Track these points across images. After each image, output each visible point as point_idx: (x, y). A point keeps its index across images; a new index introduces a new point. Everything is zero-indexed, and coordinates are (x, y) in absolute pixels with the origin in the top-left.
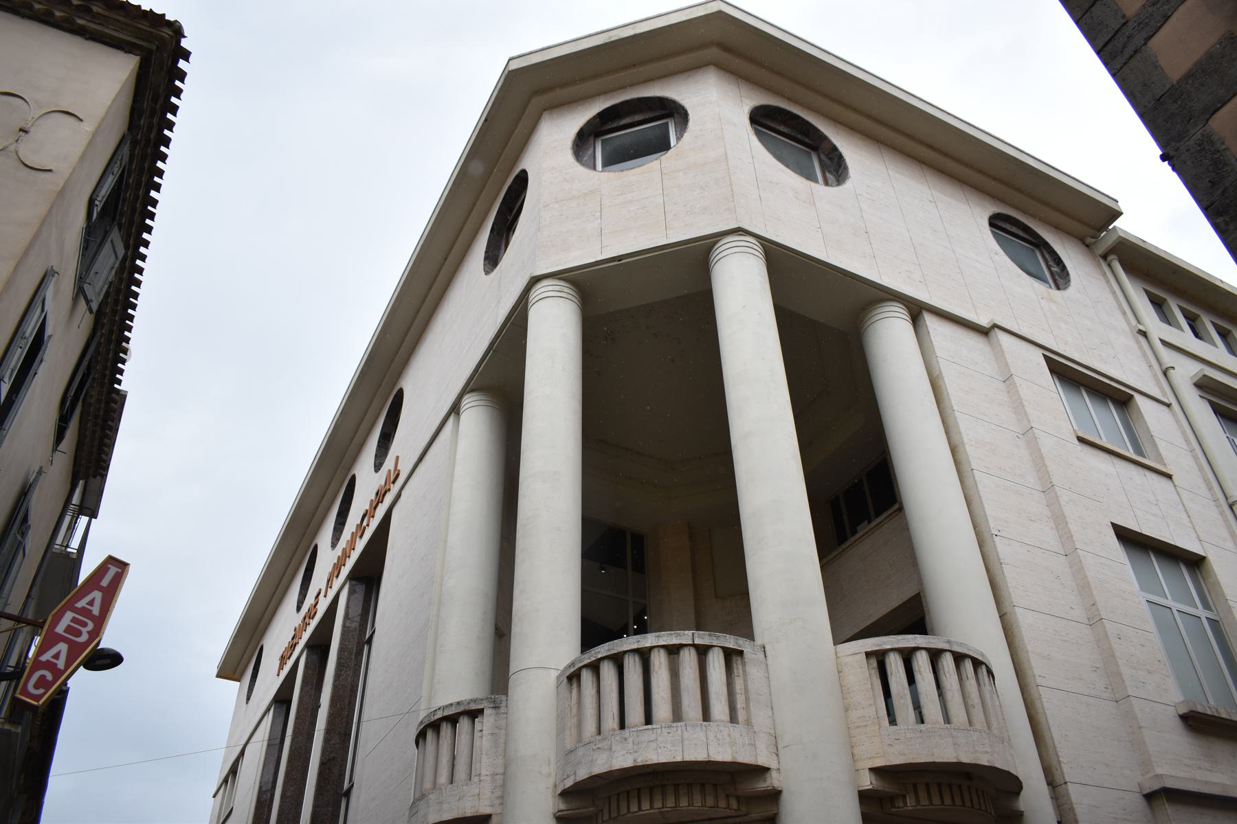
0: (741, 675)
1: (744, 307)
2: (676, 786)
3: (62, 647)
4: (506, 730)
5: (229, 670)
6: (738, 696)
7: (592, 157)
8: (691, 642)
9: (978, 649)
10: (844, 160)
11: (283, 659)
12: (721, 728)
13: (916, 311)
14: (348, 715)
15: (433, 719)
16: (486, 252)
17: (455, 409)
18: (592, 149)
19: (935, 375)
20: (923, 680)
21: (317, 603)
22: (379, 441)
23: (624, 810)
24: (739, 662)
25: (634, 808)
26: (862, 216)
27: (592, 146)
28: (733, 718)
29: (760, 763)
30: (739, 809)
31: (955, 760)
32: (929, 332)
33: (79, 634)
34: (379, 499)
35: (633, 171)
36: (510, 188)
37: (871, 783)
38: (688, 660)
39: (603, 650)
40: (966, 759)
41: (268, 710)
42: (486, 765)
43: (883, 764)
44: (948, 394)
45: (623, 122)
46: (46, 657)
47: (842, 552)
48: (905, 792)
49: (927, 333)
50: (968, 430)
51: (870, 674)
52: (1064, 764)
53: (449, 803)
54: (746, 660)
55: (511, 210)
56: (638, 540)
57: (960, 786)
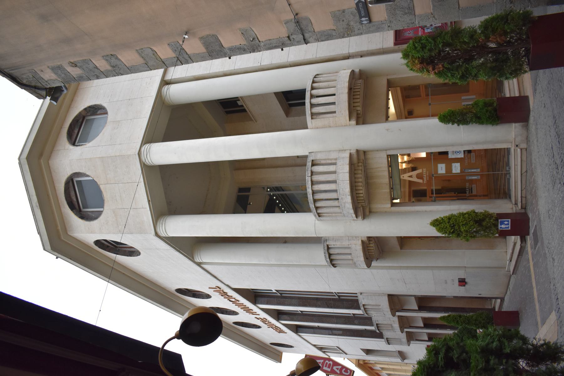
0: (320, 161)
1: (175, 153)
2: (355, 182)
3: (335, 368)
5: (277, 358)
6: (327, 162)
7: (93, 213)
8: (310, 177)
10: (91, 106)
11: (281, 331)
12: (338, 168)
14: (310, 299)
15: (329, 261)
16: (128, 256)
17: (199, 264)
18: (89, 213)
20: (321, 101)
22: (196, 298)
24: (315, 161)
26: (121, 101)
27: (87, 213)
28: (335, 164)
29: (349, 156)
30: (362, 163)
31: (347, 94)
33: (330, 364)
39: (312, 206)
41: (300, 336)
42: (346, 243)
45: (75, 199)
46: (338, 372)
47: (250, 113)
48: (356, 110)
53: (358, 254)
54: (315, 159)
55: (108, 246)
56: (241, 190)
57: (354, 92)
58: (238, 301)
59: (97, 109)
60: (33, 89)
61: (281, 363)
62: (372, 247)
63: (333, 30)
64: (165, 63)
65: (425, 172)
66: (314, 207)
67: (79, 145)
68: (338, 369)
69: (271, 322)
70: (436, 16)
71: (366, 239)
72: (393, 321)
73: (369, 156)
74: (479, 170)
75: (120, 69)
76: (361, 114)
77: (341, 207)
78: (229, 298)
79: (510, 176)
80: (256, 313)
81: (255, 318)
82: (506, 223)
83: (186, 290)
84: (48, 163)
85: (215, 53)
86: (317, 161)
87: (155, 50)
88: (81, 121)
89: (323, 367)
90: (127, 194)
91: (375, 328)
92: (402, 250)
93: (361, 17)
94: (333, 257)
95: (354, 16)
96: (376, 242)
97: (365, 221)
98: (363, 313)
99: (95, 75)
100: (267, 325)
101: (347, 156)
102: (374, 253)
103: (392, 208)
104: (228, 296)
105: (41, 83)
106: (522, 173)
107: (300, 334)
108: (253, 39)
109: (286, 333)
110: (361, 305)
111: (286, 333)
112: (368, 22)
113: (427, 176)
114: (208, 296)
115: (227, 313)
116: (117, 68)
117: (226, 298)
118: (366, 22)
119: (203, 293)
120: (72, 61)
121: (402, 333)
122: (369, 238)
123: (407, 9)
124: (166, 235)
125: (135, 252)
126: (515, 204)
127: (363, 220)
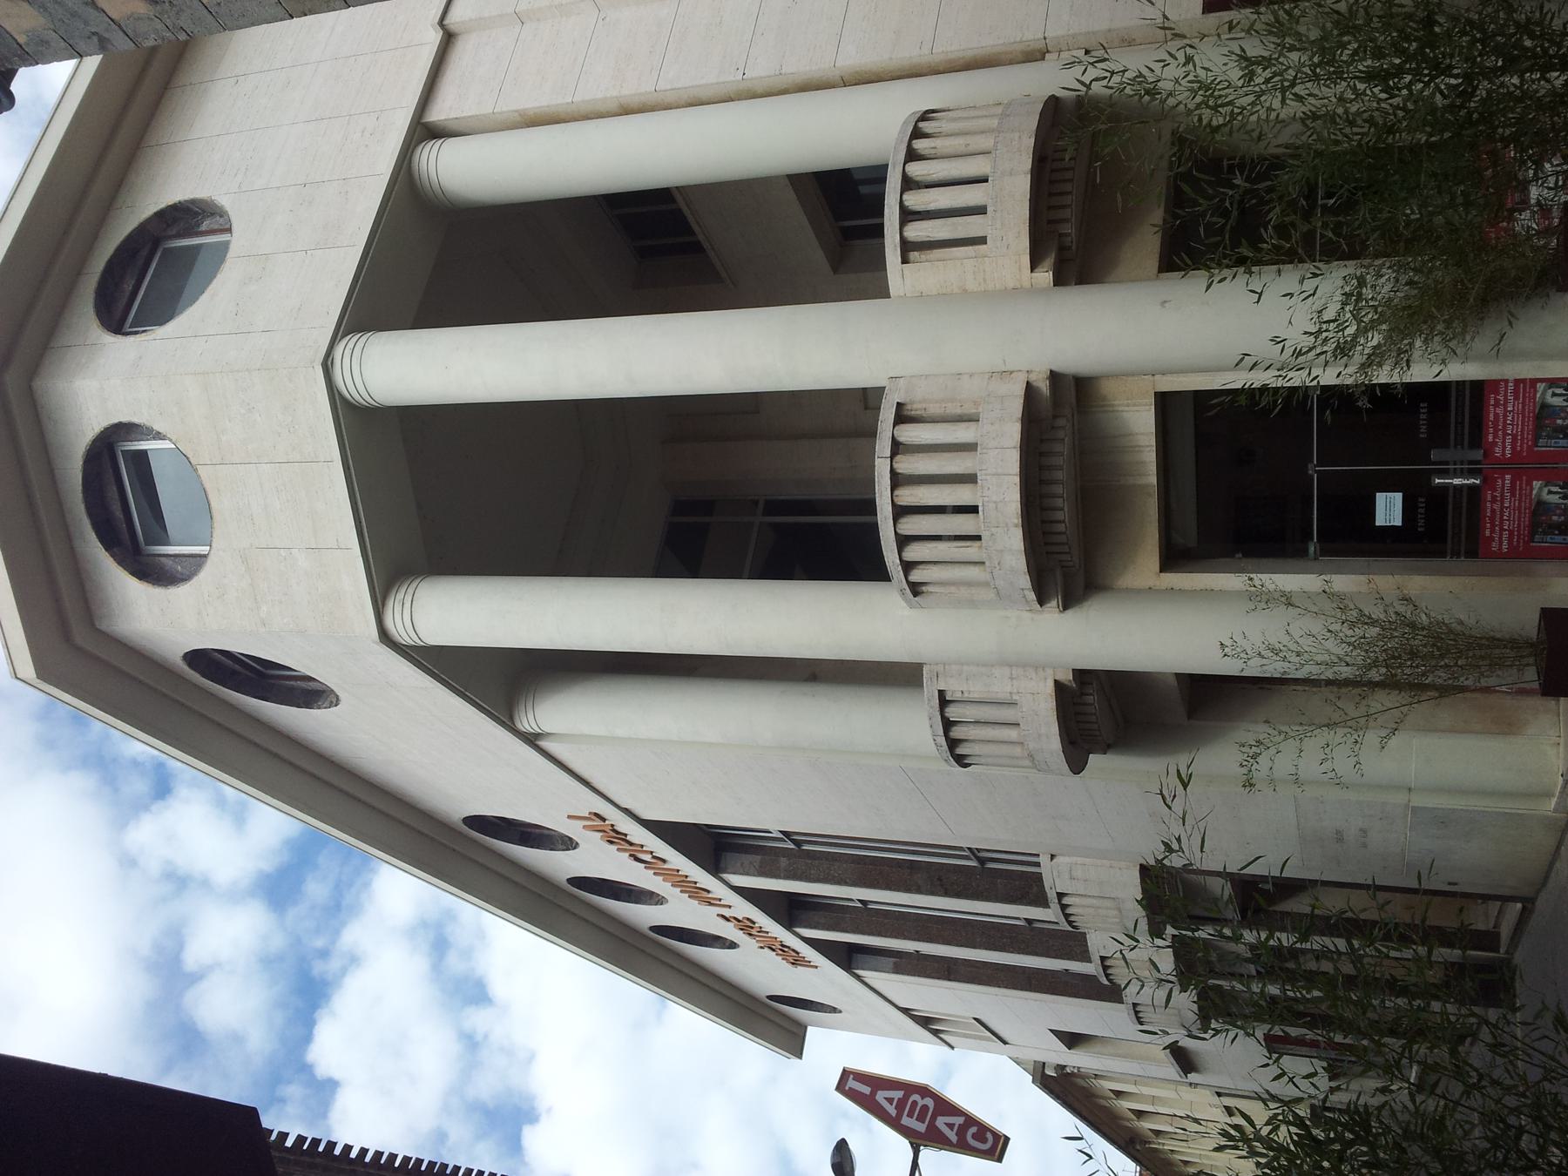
2: (1042, 482)
3: (941, 1122)
4: (962, 664)
5: (790, 1039)
9: (898, 129)
10: (180, 202)
11: (797, 961)
13: (424, 131)
17: (532, 740)
18: (163, 559)
19: (519, 119)
21: (735, 918)
22: (532, 847)
23: (1063, 538)
24: (909, 407)
25: (1061, 528)
27: (161, 558)
28: (972, 419)
29: (1022, 393)
31: (1029, 176)
32: (456, 118)
34: (623, 840)
35: (213, 504)
36: (204, 676)
37: (1047, 271)
38: (907, 465)
40: (1026, 163)
41: (858, 978)
42: (1001, 687)
43: (1027, 258)
44: (548, 106)
45: (119, 514)
46: (953, 1137)
49: (456, 121)
50: (598, 87)
51: (927, 261)
52: (1023, 36)
55: (234, 672)
57: (1052, 171)
58: (664, 861)
59: (200, 214)
61: (801, 1058)
66: (898, 561)
67: (136, 333)
68: (951, 1126)
69: (767, 933)
71: (1071, 678)
76: (1074, 248)
77: (987, 564)
78: (633, 850)
80: (720, 900)
81: (718, 915)
83: (498, 821)
84: (30, 387)
86: (915, 406)
88: (144, 253)
89: (899, 1115)
90: (288, 501)
94: (956, 733)
97: (1069, 613)
99: (94, 34)
100: (757, 941)
101: (1015, 394)
102: (1096, 726)
104: (631, 844)
107: (860, 972)
109: (816, 967)
111: (816, 967)
114: (568, 844)
115: (630, 896)
117: (625, 850)
119: (553, 833)
122: (1081, 675)
124: (419, 641)
125: (325, 694)
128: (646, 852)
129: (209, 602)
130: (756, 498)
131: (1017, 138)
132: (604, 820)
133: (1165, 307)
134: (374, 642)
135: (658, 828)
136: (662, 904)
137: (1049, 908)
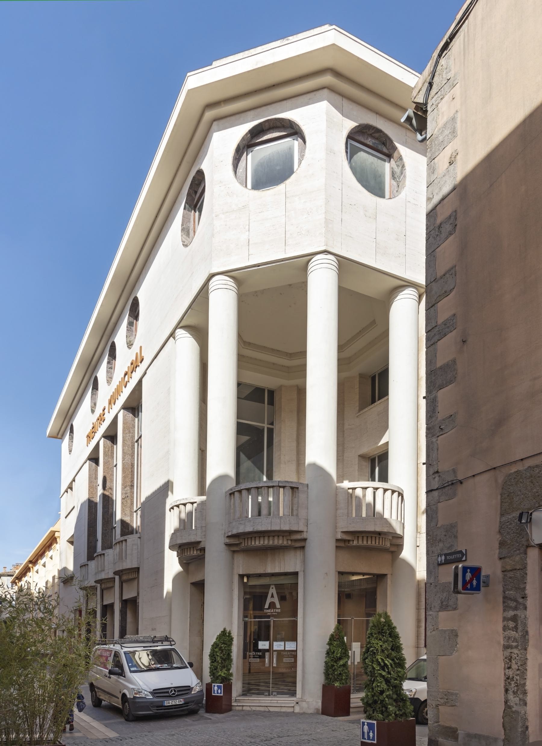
11: (90, 437)
17: (172, 335)
29: (300, 530)
31: (373, 530)
41: (85, 462)
48: (354, 539)
55: (196, 192)
58: (125, 387)
60: (429, 78)
62: (193, 553)
63: (437, 523)
64: (432, 308)
65: (277, 610)
66: (242, 488)
70: (434, 633)
72: (108, 573)
73: (299, 553)
74: (275, 665)
75: (434, 238)
79: (266, 696)
82: (219, 691)
85: (433, 378)
86: (297, 494)
87: (450, 295)
91: (99, 552)
92: (189, 585)
93: (446, 555)
95: (449, 548)
96: (199, 556)
97: (224, 546)
98: (116, 539)
102: (186, 554)
103: (238, 575)
104: (132, 373)
105: (436, 96)
106: (268, 707)
108: (442, 429)
110: (125, 537)
112: (439, 563)
113: (272, 613)
116: (437, 233)
118: (439, 560)
120: (458, 157)
121: (95, 582)
122: (203, 550)
123: (447, 604)
126: (236, 700)
127: (225, 543)
128: (128, 379)
129: (225, 187)
130: (274, 425)
131: (387, 526)
132: (141, 362)
133: (325, 574)
134: (209, 271)
135: (140, 383)
136: (107, 383)
137: (121, 537)
